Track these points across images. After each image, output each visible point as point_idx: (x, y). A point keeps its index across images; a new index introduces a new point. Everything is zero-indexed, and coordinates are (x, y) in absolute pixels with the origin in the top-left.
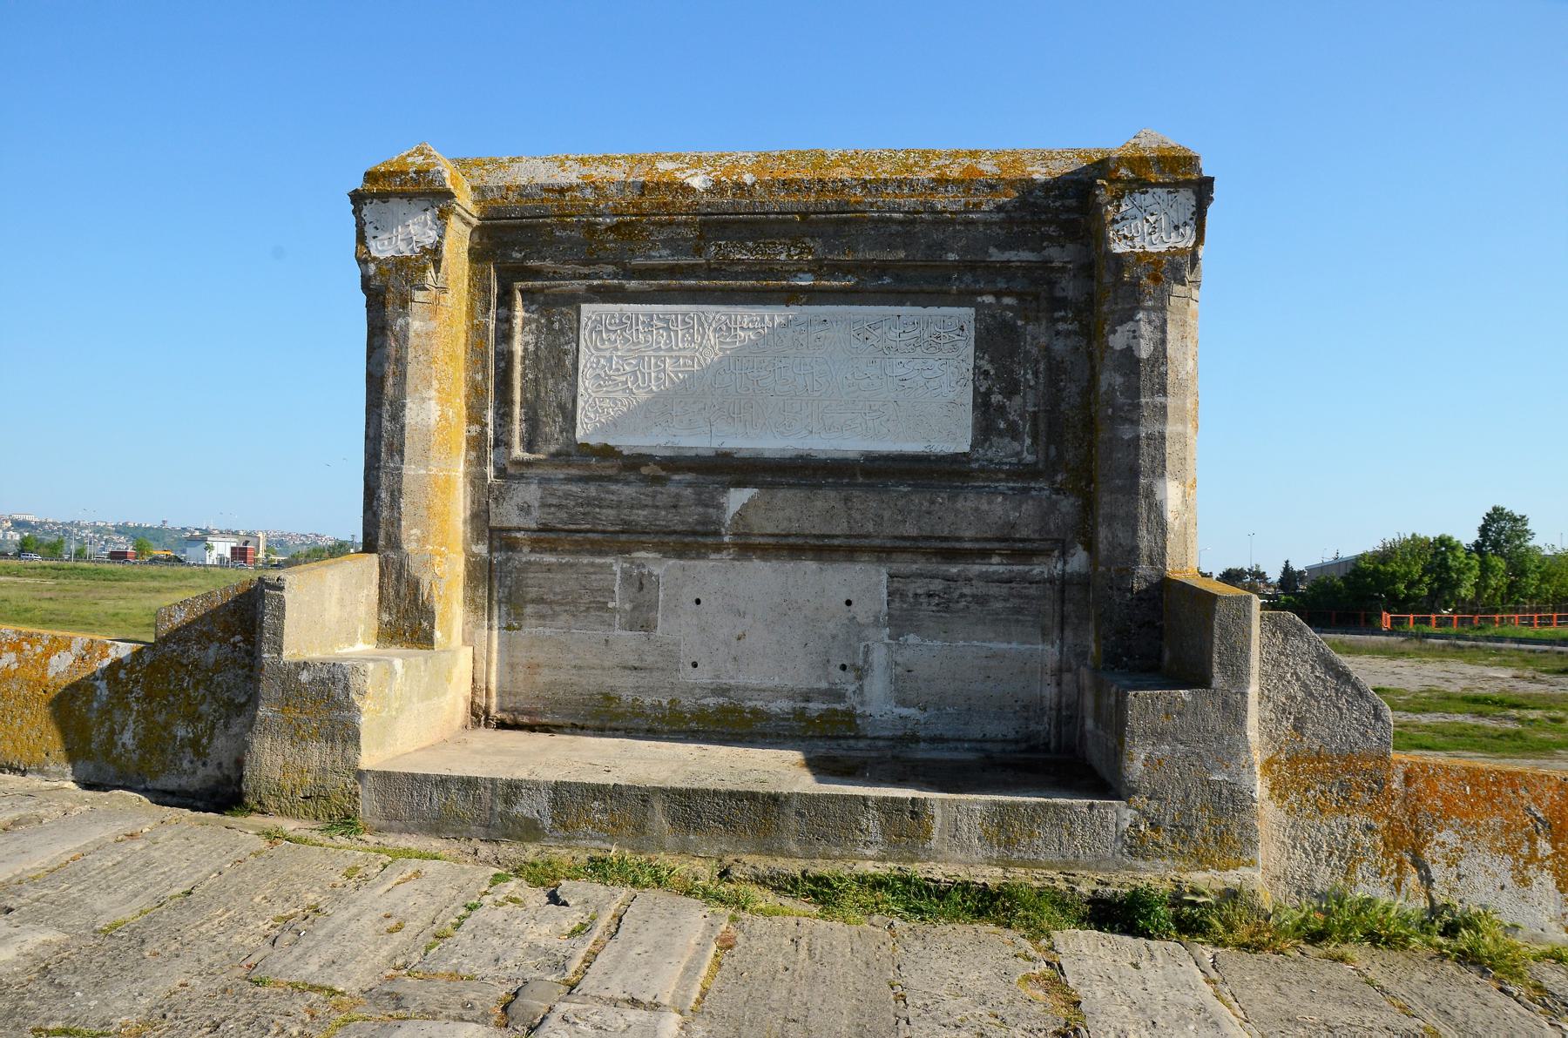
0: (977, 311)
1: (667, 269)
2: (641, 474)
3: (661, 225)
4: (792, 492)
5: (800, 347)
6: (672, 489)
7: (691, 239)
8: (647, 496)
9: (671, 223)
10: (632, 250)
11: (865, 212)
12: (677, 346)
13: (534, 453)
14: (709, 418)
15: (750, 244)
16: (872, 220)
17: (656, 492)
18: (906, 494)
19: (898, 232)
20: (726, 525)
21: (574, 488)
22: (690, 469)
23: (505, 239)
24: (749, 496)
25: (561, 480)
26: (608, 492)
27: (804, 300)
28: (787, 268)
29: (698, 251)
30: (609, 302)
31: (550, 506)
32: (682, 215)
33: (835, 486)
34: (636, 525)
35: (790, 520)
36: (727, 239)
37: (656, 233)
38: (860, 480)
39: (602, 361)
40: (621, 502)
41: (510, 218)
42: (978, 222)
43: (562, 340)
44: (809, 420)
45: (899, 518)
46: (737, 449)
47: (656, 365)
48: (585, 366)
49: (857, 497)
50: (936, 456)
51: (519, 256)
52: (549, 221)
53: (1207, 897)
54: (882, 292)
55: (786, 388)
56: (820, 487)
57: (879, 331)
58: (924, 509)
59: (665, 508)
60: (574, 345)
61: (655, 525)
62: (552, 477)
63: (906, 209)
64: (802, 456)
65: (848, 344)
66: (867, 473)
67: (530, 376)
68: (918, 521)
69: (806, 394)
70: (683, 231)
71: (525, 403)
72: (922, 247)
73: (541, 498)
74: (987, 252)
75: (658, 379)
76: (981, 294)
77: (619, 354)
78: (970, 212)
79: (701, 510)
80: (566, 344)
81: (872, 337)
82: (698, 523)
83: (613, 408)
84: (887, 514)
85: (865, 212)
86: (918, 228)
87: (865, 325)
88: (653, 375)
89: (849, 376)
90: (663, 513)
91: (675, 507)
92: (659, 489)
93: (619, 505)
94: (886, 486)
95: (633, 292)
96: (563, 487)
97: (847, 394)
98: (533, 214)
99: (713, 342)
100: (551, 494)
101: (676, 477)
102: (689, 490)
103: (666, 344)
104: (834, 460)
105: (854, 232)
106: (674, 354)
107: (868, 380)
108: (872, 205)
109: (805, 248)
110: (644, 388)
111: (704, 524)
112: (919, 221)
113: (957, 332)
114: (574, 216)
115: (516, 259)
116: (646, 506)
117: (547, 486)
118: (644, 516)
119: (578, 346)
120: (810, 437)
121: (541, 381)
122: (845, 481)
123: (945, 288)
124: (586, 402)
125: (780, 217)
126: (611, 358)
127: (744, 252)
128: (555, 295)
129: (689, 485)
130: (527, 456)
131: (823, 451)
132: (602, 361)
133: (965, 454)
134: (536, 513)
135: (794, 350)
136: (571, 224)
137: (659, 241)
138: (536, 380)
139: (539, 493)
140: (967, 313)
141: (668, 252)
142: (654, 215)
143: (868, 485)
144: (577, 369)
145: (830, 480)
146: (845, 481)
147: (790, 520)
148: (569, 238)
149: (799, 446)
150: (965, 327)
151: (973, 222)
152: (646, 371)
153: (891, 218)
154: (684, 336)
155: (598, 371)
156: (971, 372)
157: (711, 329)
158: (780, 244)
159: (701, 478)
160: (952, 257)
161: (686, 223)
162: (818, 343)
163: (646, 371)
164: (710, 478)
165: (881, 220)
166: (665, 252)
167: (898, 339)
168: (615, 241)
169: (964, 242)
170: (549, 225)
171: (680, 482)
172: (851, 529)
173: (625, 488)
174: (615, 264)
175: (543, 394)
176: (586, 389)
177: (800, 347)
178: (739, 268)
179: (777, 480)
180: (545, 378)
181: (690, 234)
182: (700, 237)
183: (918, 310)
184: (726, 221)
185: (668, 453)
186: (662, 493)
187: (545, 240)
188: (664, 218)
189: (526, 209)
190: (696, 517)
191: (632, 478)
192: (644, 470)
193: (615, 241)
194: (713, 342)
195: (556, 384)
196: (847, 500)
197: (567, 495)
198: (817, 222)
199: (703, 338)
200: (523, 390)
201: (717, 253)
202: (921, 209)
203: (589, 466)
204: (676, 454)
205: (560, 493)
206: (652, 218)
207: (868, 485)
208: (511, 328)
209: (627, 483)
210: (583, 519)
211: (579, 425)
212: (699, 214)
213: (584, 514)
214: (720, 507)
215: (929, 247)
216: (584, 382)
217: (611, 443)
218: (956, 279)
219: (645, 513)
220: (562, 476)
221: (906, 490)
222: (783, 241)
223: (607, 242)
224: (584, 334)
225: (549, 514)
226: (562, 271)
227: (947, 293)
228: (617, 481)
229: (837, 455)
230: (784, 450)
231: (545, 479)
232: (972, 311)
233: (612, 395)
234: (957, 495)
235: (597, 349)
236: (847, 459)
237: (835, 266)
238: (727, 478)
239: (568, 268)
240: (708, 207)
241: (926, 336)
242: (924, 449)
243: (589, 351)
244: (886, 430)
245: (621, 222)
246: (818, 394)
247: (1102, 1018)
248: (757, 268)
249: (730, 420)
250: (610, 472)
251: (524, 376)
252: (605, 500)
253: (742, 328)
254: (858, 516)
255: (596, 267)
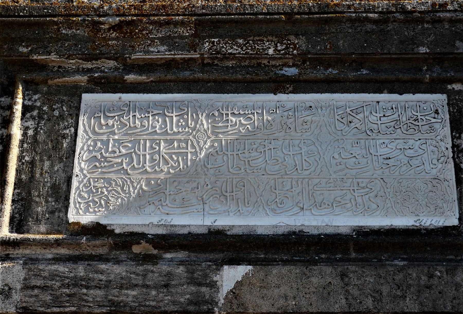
0: (449, 97)
1: (163, 65)
2: (132, 253)
3: (160, 24)
4: (287, 268)
5: (288, 131)
6: (164, 267)
7: (186, 37)
8: (138, 275)
9: (168, 23)
10: (133, 47)
11: (344, 13)
12: (172, 130)
13: (23, 233)
14: (202, 198)
15: (241, 41)
16: (350, 20)
17: (147, 271)
18: (402, 269)
19: (373, 30)
20: (220, 305)
21: (61, 268)
22: (182, 247)
23: (13, 36)
24: (243, 273)
25: (50, 260)
26: (96, 272)
27: (291, 89)
28: (274, 63)
29: (193, 47)
30: (108, 92)
31: (33, 288)
32: (179, 15)
33: (329, 262)
34: (125, 306)
35: (286, 297)
36: (220, 36)
37: (155, 32)
38: (353, 255)
39: (99, 144)
40: (110, 281)
41: (19, 16)
42: (444, 20)
43: (62, 126)
44: (300, 198)
45: (399, 293)
46: (230, 226)
47: (152, 148)
48: (82, 149)
49: (354, 272)
50: (426, 229)
51: (25, 50)
52: (56, 19)
53: (142, 185)
54: (361, 82)
55: (277, 167)
56: (315, 263)
57: (361, 115)
58: (422, 283)
59: (156, 287)
60: (73, 130)
61: (145, 306)
62: (40, 257)
63: (380, 9)
64: (294, 233)
65: (333, 127)
66: (360, 248)
67: (27, 158)
68: (418, 296)
69: (295, 173)
70: (180, 30)
71: (18, 184)
72: (396, 42)
73: (25, 279)
74: (454, 46)
75: (152, 160)
76: (451, 82)
77: (116, 137)
78: (437, 12)
79: (193, 288)
80: (65, 128)
81: (355, 120)
82: (190, 302)
83: (107, 188)
84: (385, 289)
85: (344, 13)
86: (390, 27)
87: (348, 110)
88: (148, 157)
89: (336, 156)
90: (154, 293)
91: (166, 286)
92: (150, 267)
93: (107, 285)
94: (380, 260)
95: (131, 83)
96: (50, 267)
97: (335, 172)
98: (41, 13)
99: (206, 127)
100: (35, 275)
101: (168, 256)
102: (182, 268)
103: (161, 128)
104: (327, 236)
105: (333, 30)
106: (169, 138)
107: (354, 159)
108: (349, 7)
109: (290, 44)
110: (139, 169)
111: (196, 303)
112: (392, 20)
113: (433, 115)
114: (80, 16)
115: (22, 53)
116: (136, 285)
117: (32, 267)
118: (134, 296)
119: (76, 130)
120: (301, 213)
121: (38, 163)
122: (339, 256)
123: (418, 76)
124: (80, 182)
125: (268, 17)
126: (109, 140)
127: (235, 47)
128: (59, 86)
129: (181, 263)
130: (15, 236)
131: (315, 227)
132: (99, 144)
133: (454, 227)
134: (16, 297)
135: (283, 133)
136: (77, 24)
137: (158, 38)
138: (32, 163)
139: (22, 275)
140: (440, 98)
141: (166, 48)
142: (154, 15)
143: (361, 260)
144: (74, 152)
145: (323, 256)
146: (339, 256)
147: (286, 297)
148: (74, 36)
149: (292, 223)
150: (440, 111)
151: (440, 21)
152: (142, 153)
153: (367, 18)
154: (178, 121)
155: (94, 154)
156: (450, 150)
157: (204, 115)
158: (268, 41)
159: (193, 256)
160: (423, 50)
161: (182, 23)
162: (306, 127)
163: (142, 153)
164: (203, 256)
165: (358, 20)
166: (162, 48)
167: (379, 122)
168: (117, 39)
169: (432, 37)
170: (56, 23)
171: (171, 260)
172: (350, 305)
173: (115, 267)
174: (116, 59)
175: (38, 175)
176: (82, 170)
177: (288, 131)
178: (230, 64)
179: (270, 256)
180: (42, 160)
181: (186, 32)
182: (195, 35)
183: (395, 97)
184: (218, 21)
185: (160, 231)
186: (152, 272)
187: (51, 37)
188: (162, 18)
189: (34, 8)
190: (188, 296)
191: (123, 257)
192: (136, 249)
193: (117, 39)
194: (206, 127)
195: (52, 166)
196: (343, 275)
197: (53, 276)
198: (301, 22)
199: (196, 123)
200: (19, 171)
201: (210, 49)
202: (394, 9)
203: (79, 245)
204: (168, 232)
205: (46, 274)
206: (152, 18)
207: (361, 260)
208: (12, 113)
209: (118, 262)
210: (67, 301)
211: (72, 205)
212: (195, 15)
213: (69, 295)
214: (213, 285)
215: (402, 42)
216: (80, 164)
217: (103, 222)
218: (427, 70)
219: (134, 293)
220: (50, 256)
221: (402, 263)
222: (270, 38)
223: (109, 40)
224: (83, 120)
225: (31, 296)
226: (66, 66)
227: (420, 81)
228: (107, 260)
229: (329, 231)
230: (276, 226)
231: (31, 259)
232: (444, 97)
233: (106, 176)
234: (455, 268)
235: (94, 133)
236: (339, 234)
237: (316, 59)
238: (220, 256)
239: (72, 63)
240: (203, 9)
241: (404, 119)
242: (413, 223)
243: (88, 135)
244: (375, 206)
245: (123, 21)
246: (307, 172)
247: (241, 300)
248: (247, 63)
249: (222, 198)
250: (100, 251)
251: (20, 158)
252: (93, 280)
253: (233, 114)
254: (355, 292)
255: (99, 62)
